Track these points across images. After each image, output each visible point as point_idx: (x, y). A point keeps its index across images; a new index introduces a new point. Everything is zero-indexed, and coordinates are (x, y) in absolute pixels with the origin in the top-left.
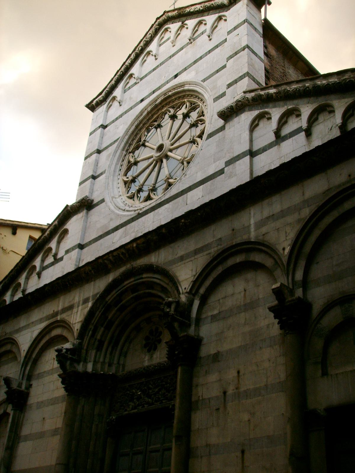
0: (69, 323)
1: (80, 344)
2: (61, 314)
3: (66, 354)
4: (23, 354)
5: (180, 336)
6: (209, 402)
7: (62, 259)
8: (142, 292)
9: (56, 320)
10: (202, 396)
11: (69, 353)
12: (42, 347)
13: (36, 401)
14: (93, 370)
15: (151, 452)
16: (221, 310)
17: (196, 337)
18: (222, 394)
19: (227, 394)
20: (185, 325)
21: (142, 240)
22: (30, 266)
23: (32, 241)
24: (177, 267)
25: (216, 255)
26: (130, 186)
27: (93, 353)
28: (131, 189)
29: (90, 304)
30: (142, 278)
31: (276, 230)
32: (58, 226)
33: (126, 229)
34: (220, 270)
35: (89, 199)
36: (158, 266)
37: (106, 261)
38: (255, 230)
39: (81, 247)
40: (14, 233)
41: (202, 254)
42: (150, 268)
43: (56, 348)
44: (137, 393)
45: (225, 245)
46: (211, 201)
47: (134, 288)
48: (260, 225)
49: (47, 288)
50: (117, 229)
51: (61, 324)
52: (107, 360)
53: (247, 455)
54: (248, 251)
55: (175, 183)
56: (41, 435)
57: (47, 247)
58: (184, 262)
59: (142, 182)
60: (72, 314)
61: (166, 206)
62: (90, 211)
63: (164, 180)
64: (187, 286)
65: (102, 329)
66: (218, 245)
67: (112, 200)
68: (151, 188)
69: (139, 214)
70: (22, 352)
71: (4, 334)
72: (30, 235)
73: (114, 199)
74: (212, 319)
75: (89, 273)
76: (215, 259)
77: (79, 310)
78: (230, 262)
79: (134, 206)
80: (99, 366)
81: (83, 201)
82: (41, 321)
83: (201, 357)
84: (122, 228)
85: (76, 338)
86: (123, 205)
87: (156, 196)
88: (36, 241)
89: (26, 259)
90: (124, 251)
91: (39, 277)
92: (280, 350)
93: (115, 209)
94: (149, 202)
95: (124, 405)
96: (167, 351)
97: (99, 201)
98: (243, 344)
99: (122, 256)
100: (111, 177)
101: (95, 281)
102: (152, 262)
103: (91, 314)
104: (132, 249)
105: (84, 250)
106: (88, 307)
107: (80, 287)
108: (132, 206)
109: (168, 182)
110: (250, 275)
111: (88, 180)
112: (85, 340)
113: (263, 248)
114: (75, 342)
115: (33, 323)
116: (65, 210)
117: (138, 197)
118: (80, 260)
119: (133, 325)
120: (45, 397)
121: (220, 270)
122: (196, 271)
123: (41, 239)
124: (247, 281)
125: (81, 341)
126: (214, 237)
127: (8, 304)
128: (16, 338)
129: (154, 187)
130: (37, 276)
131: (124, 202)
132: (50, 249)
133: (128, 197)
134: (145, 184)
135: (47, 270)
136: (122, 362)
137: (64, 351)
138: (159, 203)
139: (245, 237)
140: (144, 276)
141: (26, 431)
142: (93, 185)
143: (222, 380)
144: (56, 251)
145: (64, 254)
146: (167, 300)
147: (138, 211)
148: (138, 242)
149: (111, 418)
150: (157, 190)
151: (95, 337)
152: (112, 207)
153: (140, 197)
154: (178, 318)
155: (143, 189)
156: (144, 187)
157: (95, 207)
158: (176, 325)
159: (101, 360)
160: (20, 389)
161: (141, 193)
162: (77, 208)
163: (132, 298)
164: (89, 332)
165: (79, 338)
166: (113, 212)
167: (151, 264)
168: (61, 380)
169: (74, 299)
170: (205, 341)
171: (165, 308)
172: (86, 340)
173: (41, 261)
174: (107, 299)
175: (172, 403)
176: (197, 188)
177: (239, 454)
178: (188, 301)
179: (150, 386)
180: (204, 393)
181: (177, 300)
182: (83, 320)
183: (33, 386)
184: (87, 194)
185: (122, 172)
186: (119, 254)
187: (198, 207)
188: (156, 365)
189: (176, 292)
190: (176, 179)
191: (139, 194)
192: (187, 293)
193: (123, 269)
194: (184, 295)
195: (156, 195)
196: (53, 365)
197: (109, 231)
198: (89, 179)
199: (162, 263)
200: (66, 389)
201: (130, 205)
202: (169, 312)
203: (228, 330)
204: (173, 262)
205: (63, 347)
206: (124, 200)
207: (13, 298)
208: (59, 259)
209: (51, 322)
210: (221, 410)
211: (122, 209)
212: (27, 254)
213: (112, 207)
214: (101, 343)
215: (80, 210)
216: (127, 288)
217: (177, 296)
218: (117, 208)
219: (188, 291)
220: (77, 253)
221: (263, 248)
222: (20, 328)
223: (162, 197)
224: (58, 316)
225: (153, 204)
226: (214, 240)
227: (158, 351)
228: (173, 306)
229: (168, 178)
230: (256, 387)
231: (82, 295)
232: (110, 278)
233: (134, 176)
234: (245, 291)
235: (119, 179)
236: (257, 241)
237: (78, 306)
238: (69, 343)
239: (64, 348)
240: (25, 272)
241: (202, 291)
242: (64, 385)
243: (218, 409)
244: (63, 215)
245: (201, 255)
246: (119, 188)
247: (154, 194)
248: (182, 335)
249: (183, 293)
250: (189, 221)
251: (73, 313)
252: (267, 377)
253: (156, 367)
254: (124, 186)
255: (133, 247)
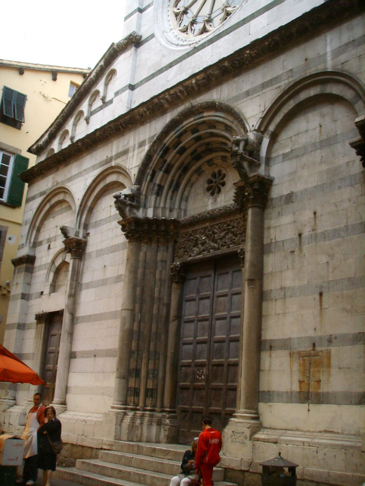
0: (125, 168)
1: (139, 189)
2: (115, 159)
3: (125, 201)
4: (78, 202)
5: (250, 176)
6: (283, 244)
7: (111, 102)
8: (204, 132)
9: (110, 166)
10: (275, 239)
11: (127, 199)
12: (98, 194)
13: (95, 249)
14: (153, 216)
15: (219, 296)
16: (293, 148)
17: (267, 178)
18: (297, 236)
19: (303, 236)
20: (254, 165)
21: (202, 75)
22: (76, 113)
23: (74, 87)
24: (242, 103)
25: (286, 88)
26: (182, 19)
27: (152, 198)
28: (183, 21)
29: (147, 148)
30: (203, 117)
31: (357, 57)
32: (104, 67)
33: (181, 65)
34: (291, 104)
35: (137, 35)
36: (220, 103)
37: (162, 101)
38: (333, 59)
39: (132, 87)
40: (55, 79)
41: (271, 87)
42: (212, 106)
43: (114, 194)
44: (201, 238)
45: (297, 77)
46: (281, 28)
47: (194, 129)
48: (337, 52)
49: (98, 133)
50: (170, 65)
51: (117, 170)
52: (168, 206)
53: (325, 297)
54: (324, 82)
55: (234, 11)
56: (103, 282)
57: (93, 90)
58: (250, 97)
59: (195, 13)
60: (127, 159)
61: (226, 37)
62: (139, 48)
63: (221, 9)
64: (255, 124)
65: (161, 173)
66: (289, 77)
67: (163, 35)
68: (206, 19)
69: (195, 48)
70: (76, 200)
71: (56, 183)
72: (71, 81)
73: (165, 34)
74: (283, 158)
75: (144, 114)
76: (285, 93)
77: (135, 155)
78: (303, 96)
79: (188, 40)
80: (160, 212)
81: (130, 38)
82: (94, 167)
83: (272, 198)
84: (176, 64)
85: (133, 183)
86: (176, 40)
87: (212, 27)
88: (79, 87)
89: (72, 104)
90: (182, 88)
91: (88, 123)
92: (362, 189)
93: (166, 44)
94: (205, 35)
95: (188, 250)
96: (235, 193)
97: (149, 37)
98: (319, 184)
99: (179, 94)
100: (160, 9)
101: (150, 122)
102: (213, 100)
103: (148, 158)
104: (191, 85)
105: (135, 90)
106: (144, 150)
107: (135, 130)
108: (186, 40)
109: (226, 10)
110: (326, 109)
111: (134, 13)
112: (143, 185)
113: (342, 79)
114: (133, 188)
115: (85, 170)
116: (112, 48)
117: (192, 29)
118: (131, 102)
119: (194, 168)
120: (104, 245)
121: (291, 104)
122: (265, 106)
123: (87, 82)
124: (323, 116)
125: (139, 186)
126: (284, 67)
127: (57, 153)
128: (68, 187)
129: (210, 18)
130: (85, 121)
131: (176, 36)
132: (98, 92)
133: (181, 31)
134: (199, 15)
135: (96, 114)
136: (183, 207)
137: (123, 197)
138: (218, 35)
139: (320, 68)
140: (205, 114)
141: (86, 278)
142: (140, 19)
143: (296, 222)
144: (104, 93)
145: (113, 97)
146: (235, 138)
147: (194, 45)
148: (198, 77)
149: (175, 263)
150: (213, 21)
151: (154, 181)
152: (164, 43)
153: (194, 30)
154: (247, 157)
155: (197, 21)
156: (198, 18)
157: (144, 44)
158: (245, 164)
159: (162, 205)
160: (78, 238)
161: (195, 25)
162: (125, 45)
163: (192, 139)
164: (148, 176)
165: (137, 183)
166: (165, 47)
167: (212, 101)
168: (121, 227)
169: (128, 143)
170: (276, 182)
171: (233, 147)
172: (145, 185)
173: (88, 106)
174: (165, 141)
175: (241, 248)
176: (261, 15)
177: (317, 297)
178: (256, 139)
179: (216, 231)
180: (277, 235)
181: (245, 138)
182: (140, 164)
183: (91, 234)
184: (134, 29)
185: (172, 2)
186: (176, 92)
187: (266, 36)
188: (222, 209)
189: (242, 130)
190: (235, 7)
191: (193, 26)
192: (255, 130)
193: (181, 109)
194: (252, 132)
195: (212, 26)
196: (110, 212)
197: (162, 68)
198: (135, 13)
199: (225, 100)
200: (127, 236)
201: (184, 39)
202: (238, 150)
203: (303, 169)
204: (237, 98)
205: (121, 193)
206: (177, 34)
207: (61, 147)
208: (107, 102)
209: (104, 169)
210: (297, 253)
211: (175, 44)
212: (73, 99)
213: (164, 43)
214: (160, 187)
215: (128, 48)
216: (187, 128)
217: (244, 133)
218: (169, 43)
219: (256, 128)
220: (127, 94)
221: (342, 79)
222: (72, 177)
223: (220, 27)
224: (112, 161)
225: (210, 36)
226: (284, 71)
227: (222, 194)
228: (242, 145)
229: (226, 7)
230: (335, 229)
231: (137, 138)
232: (168, 118)
233: (186, 6)
234: (321, 126)
235: (169, 11)
236: (334, 71)
237: (134, 150)
238: (127, 189)
239: (122, 194)
240: (72, 118)
241: (272, 128)
242: (125, 232)
243: (293, 252)
244: (109, 54)
245: (270, 88)
246: (169, 21)
247: (210, 25)
248: (252, 175)
249: (250, 131)
250: (255, 51)
251: (129, 157)
252: (347, 218)
253: (222, 211)
254: (175, 19)
255: (192, 84)
